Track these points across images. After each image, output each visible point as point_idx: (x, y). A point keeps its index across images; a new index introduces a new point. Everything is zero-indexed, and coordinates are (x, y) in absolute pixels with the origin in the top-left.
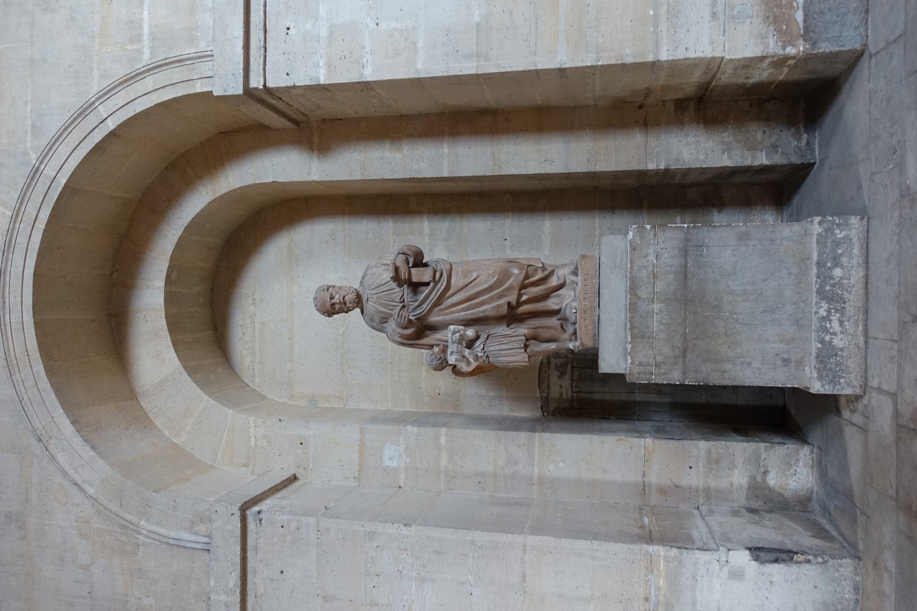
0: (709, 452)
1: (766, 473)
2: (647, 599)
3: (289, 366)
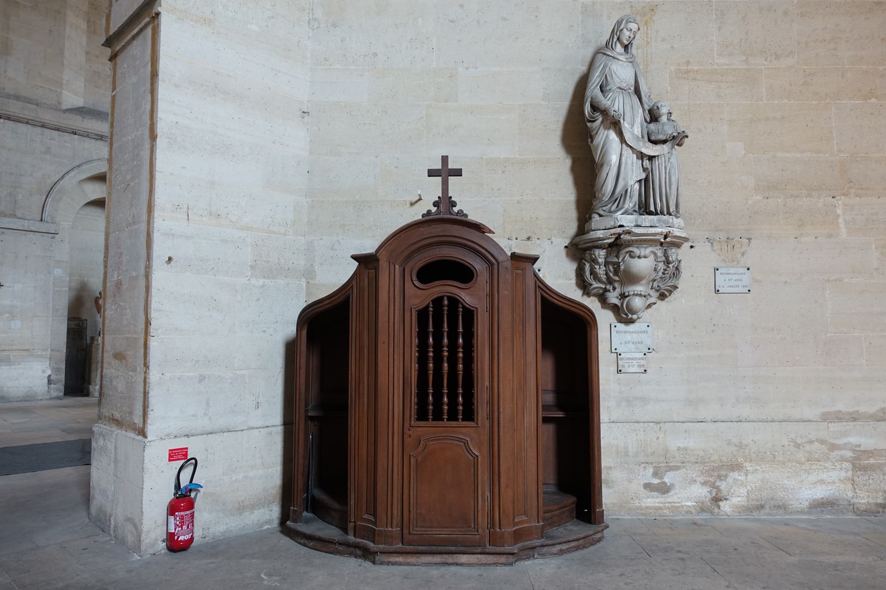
0: (61, 368)
1: (55, 384)
2: (33, 349)
3: (80, 228)
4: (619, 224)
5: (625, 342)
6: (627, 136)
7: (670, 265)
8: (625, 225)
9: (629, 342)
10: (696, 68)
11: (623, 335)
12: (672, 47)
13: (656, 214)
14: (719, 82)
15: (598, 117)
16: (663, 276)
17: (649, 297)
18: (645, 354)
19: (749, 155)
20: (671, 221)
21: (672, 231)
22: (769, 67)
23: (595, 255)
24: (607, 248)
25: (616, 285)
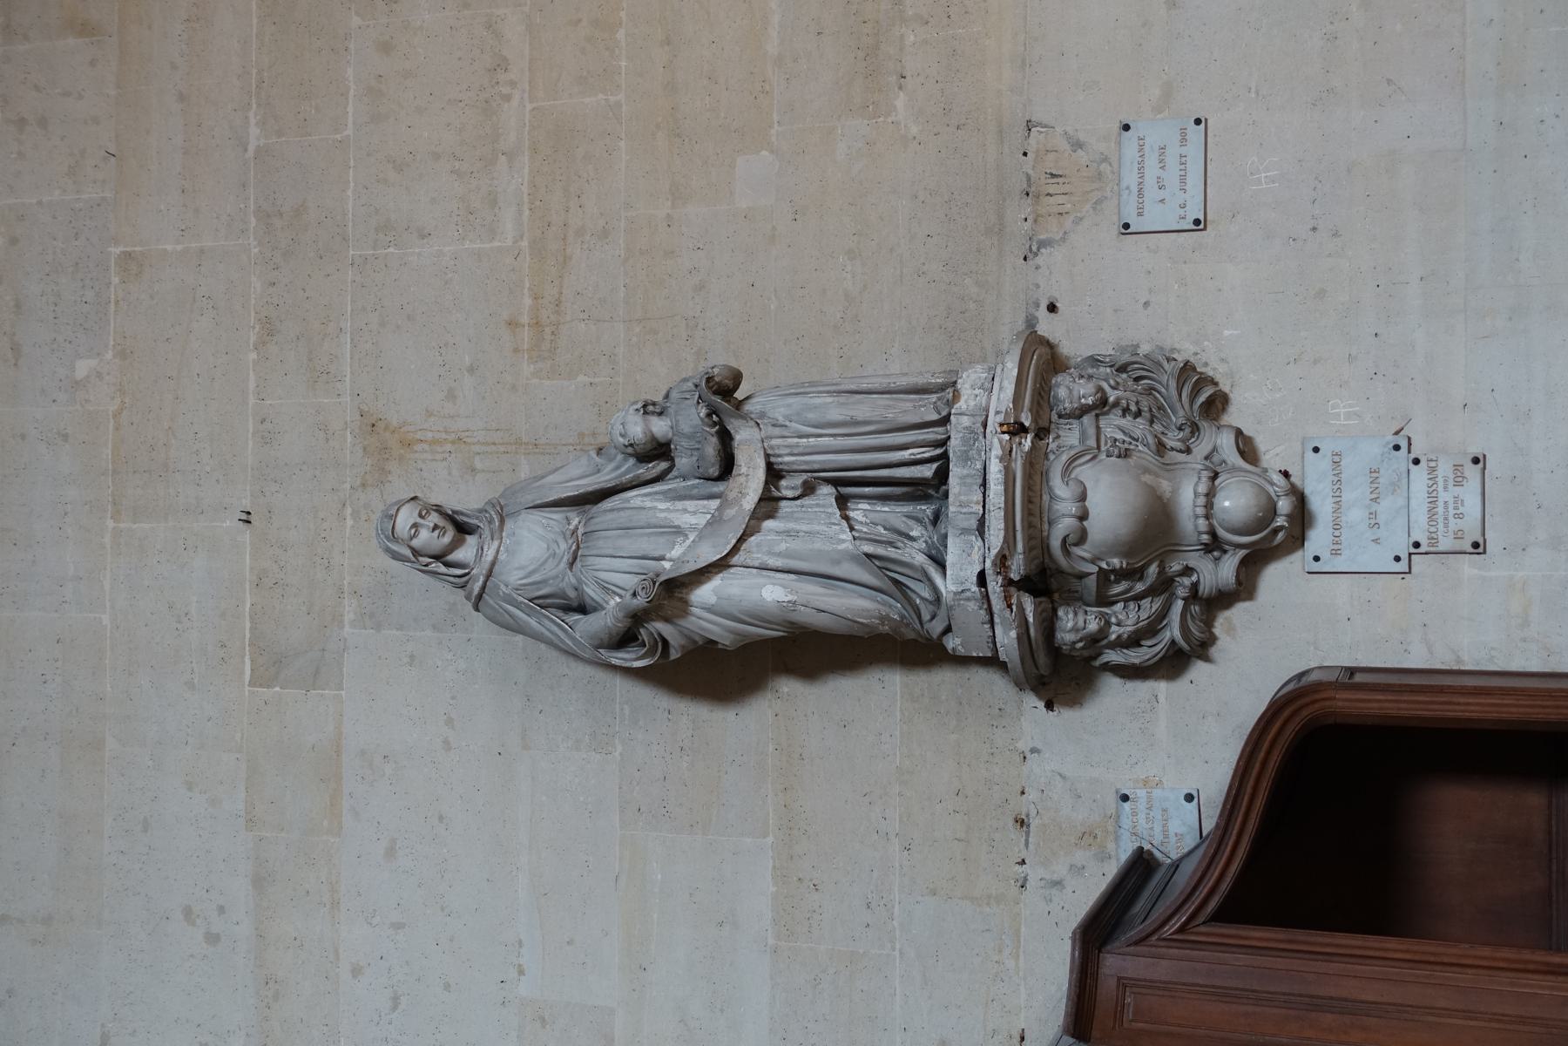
4: (975, 588)
5: (1371, 527)
6: (709, 554)
7: (1111, 399)
8: (978, 569)
9: (1373, 514)
10: (528, 301)
11: (1345, 534)
12: (471, 370)
13: (944, 457)
14: (565, 235)
15: (653, 630)
16: (1146, 414)
17: (1216, 459)
18: (1416, 462)
19: (774, 139)
20: (966, 421)
21: (1000, 418)
22: (527, 88)
23: (1074, 643)
24: (1052, 602)
25: (1176, 567)
